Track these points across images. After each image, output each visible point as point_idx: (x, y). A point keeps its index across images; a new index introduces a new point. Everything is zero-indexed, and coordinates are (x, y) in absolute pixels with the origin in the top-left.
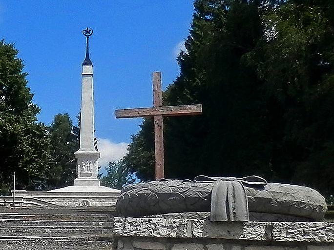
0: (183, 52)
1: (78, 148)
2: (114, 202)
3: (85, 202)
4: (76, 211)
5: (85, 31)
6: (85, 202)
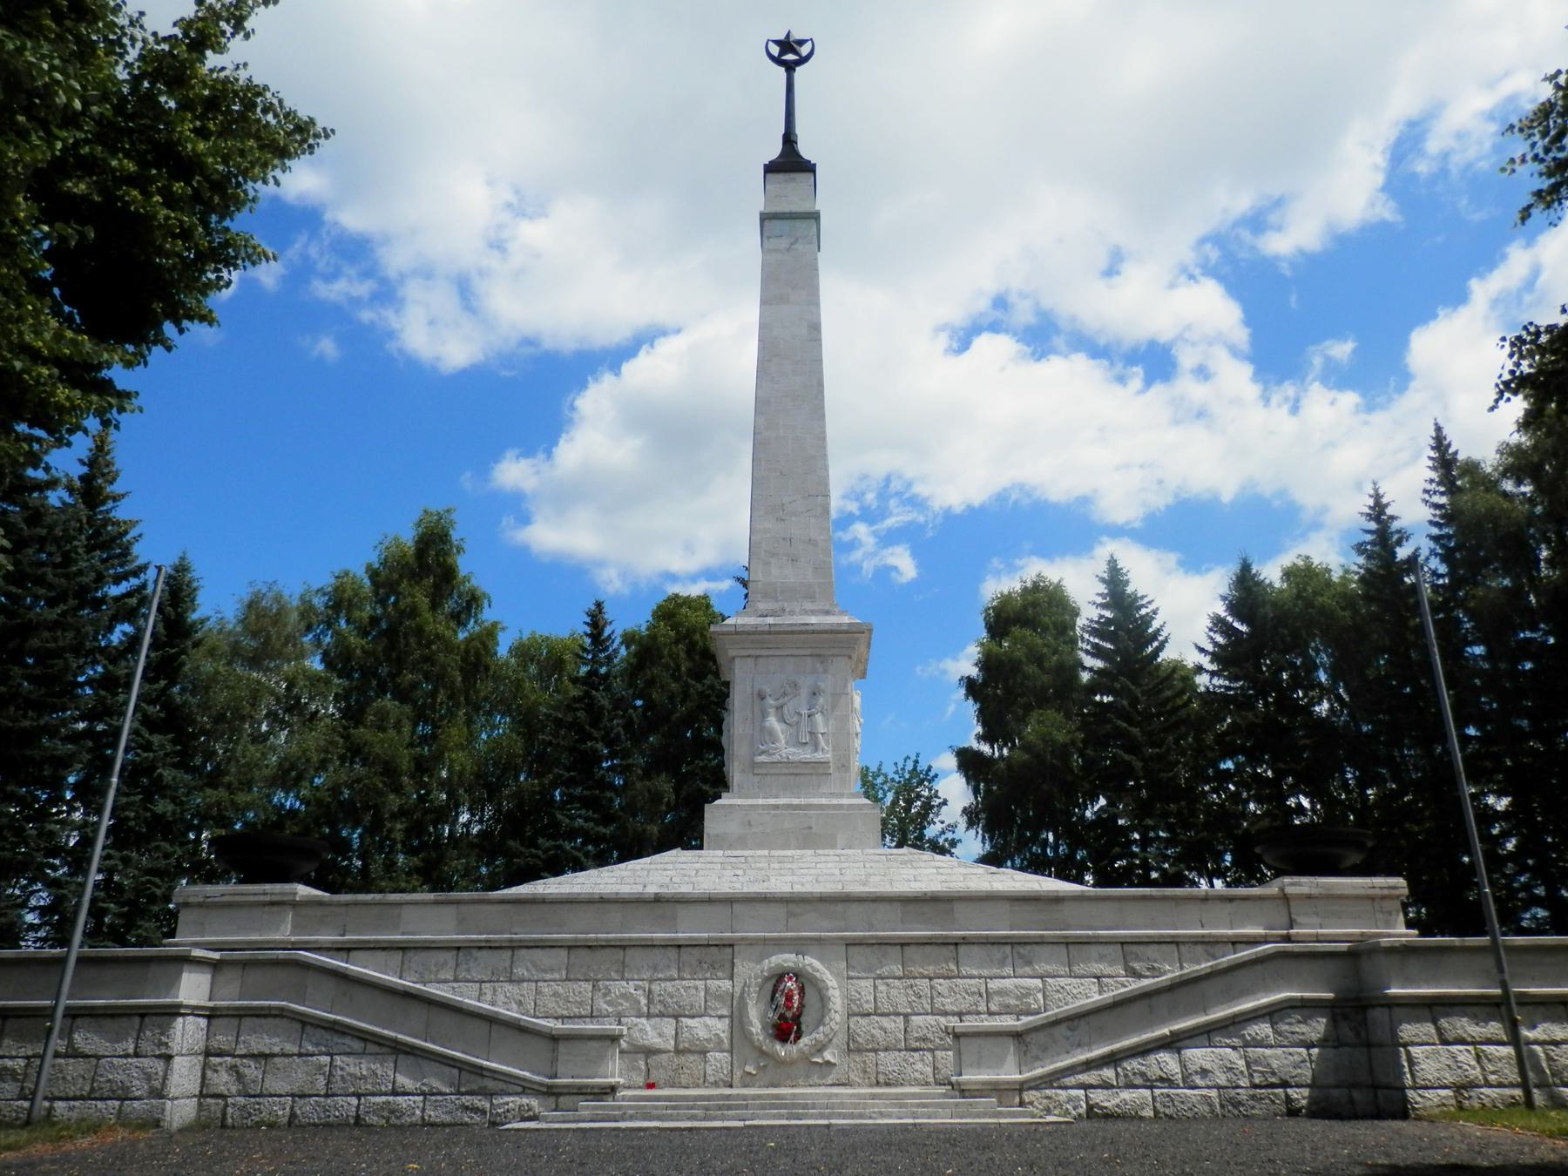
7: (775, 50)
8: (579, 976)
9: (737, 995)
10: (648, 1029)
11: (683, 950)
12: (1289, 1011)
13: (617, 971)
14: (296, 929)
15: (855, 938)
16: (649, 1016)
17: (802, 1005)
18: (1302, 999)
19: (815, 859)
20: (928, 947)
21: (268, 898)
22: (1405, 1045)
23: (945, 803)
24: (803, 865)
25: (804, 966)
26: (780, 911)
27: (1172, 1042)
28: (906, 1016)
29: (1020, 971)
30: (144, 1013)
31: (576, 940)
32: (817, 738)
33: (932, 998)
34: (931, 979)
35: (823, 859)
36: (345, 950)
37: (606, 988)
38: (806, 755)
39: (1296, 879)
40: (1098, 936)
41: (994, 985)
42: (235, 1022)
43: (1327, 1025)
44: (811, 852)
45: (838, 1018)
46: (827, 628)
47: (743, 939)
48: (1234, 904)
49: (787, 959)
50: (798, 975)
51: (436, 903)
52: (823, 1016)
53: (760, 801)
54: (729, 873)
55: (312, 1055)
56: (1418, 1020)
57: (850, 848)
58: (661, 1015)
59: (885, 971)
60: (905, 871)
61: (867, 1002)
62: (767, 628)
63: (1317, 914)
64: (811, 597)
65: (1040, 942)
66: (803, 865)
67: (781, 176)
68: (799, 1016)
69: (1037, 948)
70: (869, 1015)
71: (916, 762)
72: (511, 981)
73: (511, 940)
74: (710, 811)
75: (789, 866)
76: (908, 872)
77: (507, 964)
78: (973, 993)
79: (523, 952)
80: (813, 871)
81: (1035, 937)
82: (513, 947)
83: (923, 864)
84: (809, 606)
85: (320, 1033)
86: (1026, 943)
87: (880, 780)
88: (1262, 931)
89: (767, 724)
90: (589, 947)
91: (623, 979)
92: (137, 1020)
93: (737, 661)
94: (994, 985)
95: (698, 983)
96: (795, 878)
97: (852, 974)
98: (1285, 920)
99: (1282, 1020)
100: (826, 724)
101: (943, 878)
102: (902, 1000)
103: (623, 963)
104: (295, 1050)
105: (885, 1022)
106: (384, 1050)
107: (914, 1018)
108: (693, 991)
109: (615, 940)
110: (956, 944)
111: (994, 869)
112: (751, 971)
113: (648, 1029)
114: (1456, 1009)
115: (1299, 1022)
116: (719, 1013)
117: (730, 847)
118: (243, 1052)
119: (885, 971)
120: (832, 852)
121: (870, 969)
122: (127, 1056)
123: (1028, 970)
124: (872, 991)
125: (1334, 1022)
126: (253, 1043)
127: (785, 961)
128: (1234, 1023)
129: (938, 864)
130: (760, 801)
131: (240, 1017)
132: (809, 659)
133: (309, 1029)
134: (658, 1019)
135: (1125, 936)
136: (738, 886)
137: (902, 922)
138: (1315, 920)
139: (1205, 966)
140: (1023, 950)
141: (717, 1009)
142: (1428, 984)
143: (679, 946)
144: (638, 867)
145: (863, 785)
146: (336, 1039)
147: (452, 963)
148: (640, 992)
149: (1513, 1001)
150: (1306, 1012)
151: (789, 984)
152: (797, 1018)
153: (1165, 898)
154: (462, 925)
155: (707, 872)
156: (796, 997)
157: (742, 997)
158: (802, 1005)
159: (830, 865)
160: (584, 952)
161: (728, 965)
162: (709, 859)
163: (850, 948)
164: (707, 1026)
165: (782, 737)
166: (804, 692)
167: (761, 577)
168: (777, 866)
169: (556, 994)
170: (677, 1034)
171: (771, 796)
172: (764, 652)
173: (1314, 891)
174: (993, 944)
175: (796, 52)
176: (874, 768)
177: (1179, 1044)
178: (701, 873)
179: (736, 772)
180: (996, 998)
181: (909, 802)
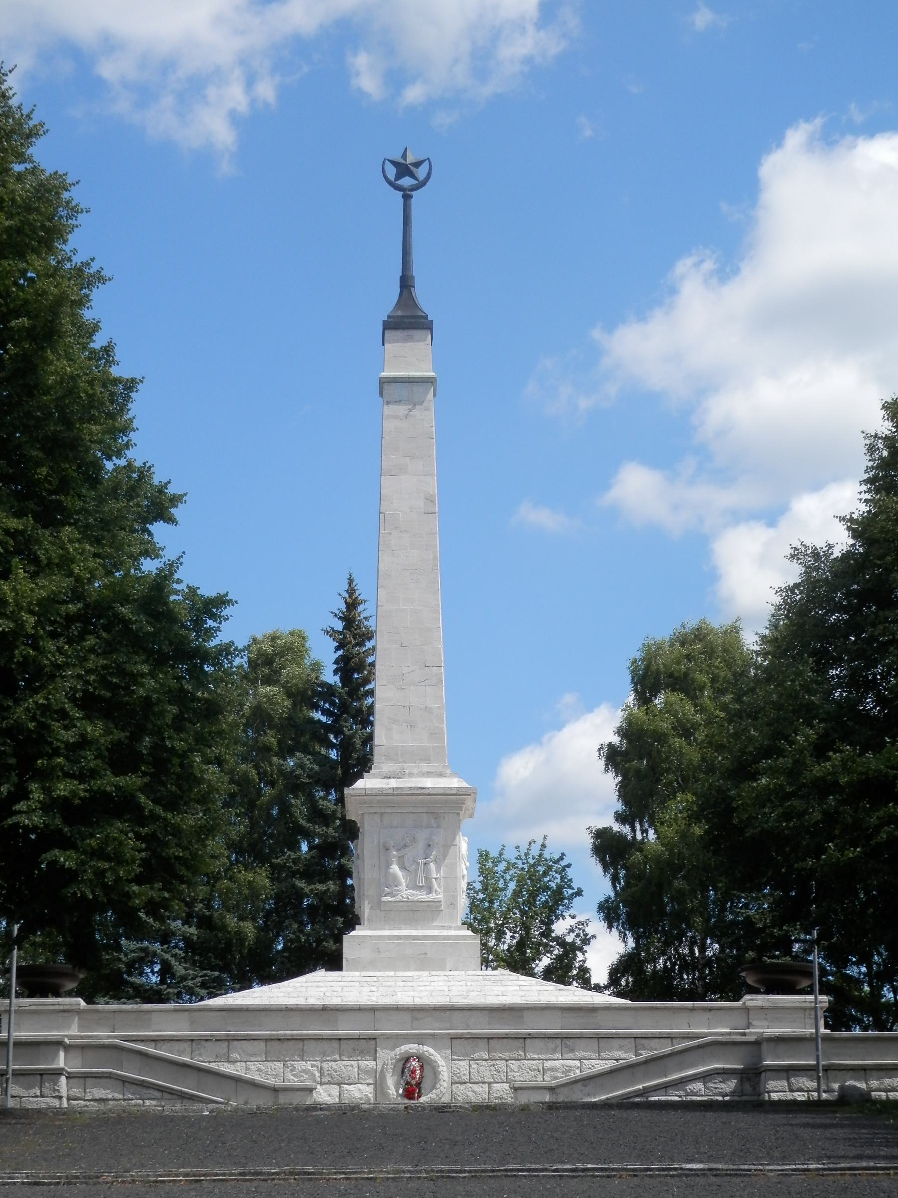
0: (11, 89)
1: (364, 764)
2: (731, 1085)
3: (414, 1063)
4: (790, 1172)
5: (394, 163)
6: (414, 1063)
7: (391, 172)
8: (273, 1059)
9: (379, 1070)
10: (322, 1091)
11: (342, 1042)
12: (716, 1075)
13: (299, 1056)
14: (81, 1027)
15: (457, 1034)
16: (321, 1084)
17: (421, 1077)
18: (724, 1069)
19: (429, 979)
20: (505, 1040)
21: (61, 1008)
22: (769, 1092)
23: (579, 892)
24: (421, 984)
25: (423, 1052)
26: (407, 1017)
27: (644, 1093)
28: (490, 1083)
29: (566, 1056)
30: (42, 1074)
31: (271, 1035)
32: (431, 882)
33: (507, 1073)
34: (507, 1061)
35: (435, 978)
36: (142, 1040)
37: (293, 1066)
38: (422, 896)
39: (754, 996)
40: (619, 1034)
41: (548, 1064)
42: (82, 1081)
43: (737, 1084)
44: (426, 973)
45: (445, 1084)
46: (440, 791)
47: (382, 1035)
48: (713, 1012)
49: (412, 1048)
50: (419, 1058)
51: (176, 1011)
52: (436, 1083)
53: (387, 933)
54: (366, 990)
55: (132, 1100)
56: (780, 1079)
57: (456, 970)
58: (329, 1083)
59: (476, 1056)
60: (496, 989)
61: (464, 1075)
62: (390, 792)
63: (766, 1019)
64: (427, 760)
65: (580, 1037)
66: (421, 984)
67: (399, 334)
68: (420, 1084)
69: (578, 1041)
70: (465, 1083)
71: (544, 846)
72: (229, 1062)
73: (228, 1035)
74: (345, 938)
75: (410, 984)
76: (498, 989)
77: (226, 1050)
78: (534, 1070)
79: (236, 1043)
80: (428, 988)
81: (576, 1033)
82: (229, 1040)
83: (510, 983)
84: (425, 767)
85: (134, 1088)
86: (571, 1038)
87: (502, 866)
88: (728, 1030)
89: (391, 870)
90: (280, 1040)
91: (303, 1060)
92: (39, 1077)
93: (366, 816)
94: (548, 1064)
95: (353, 1063)
96: (415, 994)
97: (455, 1057)
98: (744, 1023)
99: (710, 1081)
100: (438, 870)
101: (523, 993)
102: (487, 1074)
103: (303, 1050)
104: (121, 1097)
105: (475, 1087)
106: (174, 1097)
107: (495, 1085)
108: (351, 1068)
109: (297, 1035)
110: (525, 1038)
111: (562, 987)
112: (387, 1056)
113: (322, 1091)
114: (801, 1072)
115: (721, 1082)
116: (367, 1081)
117: (364, 969)
118: (90, 1097)
119: (476, 1056)
120: (442, 973)
121: (466, 1055)
122: (37, 1096)
123: (571, 1055)
124: (468, 1068)
125: (741, 1082)
126: (95, 1093)
127: (410, 1049)
128: (681, 1082)
129: (521, 983)
130: (387, 933)
131: (85, 1078)
132: (425, 815)
133: (126, 1084)
134: (327, 1085)
135: (637, 1033)
136: (374, 999)
137: (489, 1024)
138: (765, 1023)
139: (668, 1049)
140: (569, 1042)
141: (366, 1079)
142: (789, 1059)
143: (340, 1039)
144: (298, 985)
145: (482, 873)
146: (144, 1091)
147: (189, 1050)
148: (314, 1068)
149: (821, 1068)
150: (725, 1076)
151: (413, 1063)
152: (418, 1084)
153: (665, 1009)
154: (193, 1026)
155: (350, 989)
156: (418, 1072)
157: (382, 1072)
158: (421, 1077)
159: (440, 984)
160: (276, 1043)
161: (373, 1052)
162: (350, 979)
163: (454, 1040)
164: (359, 1090)
165: (403, 881)
166: (421, 845)
167: (384, 742)
168: (401, 984)
169: (259, 1070)
170: (340, 1094)
171: (394, 929)
172: (389, 810)
173: (765, 1004)
174: (549, 1038)
175: (413, 176)
176: (494, 853)
177: (647, 1094)
178: (345, 989)
179: (365, 909)
180: (549, 1072)
181: (533, 895)
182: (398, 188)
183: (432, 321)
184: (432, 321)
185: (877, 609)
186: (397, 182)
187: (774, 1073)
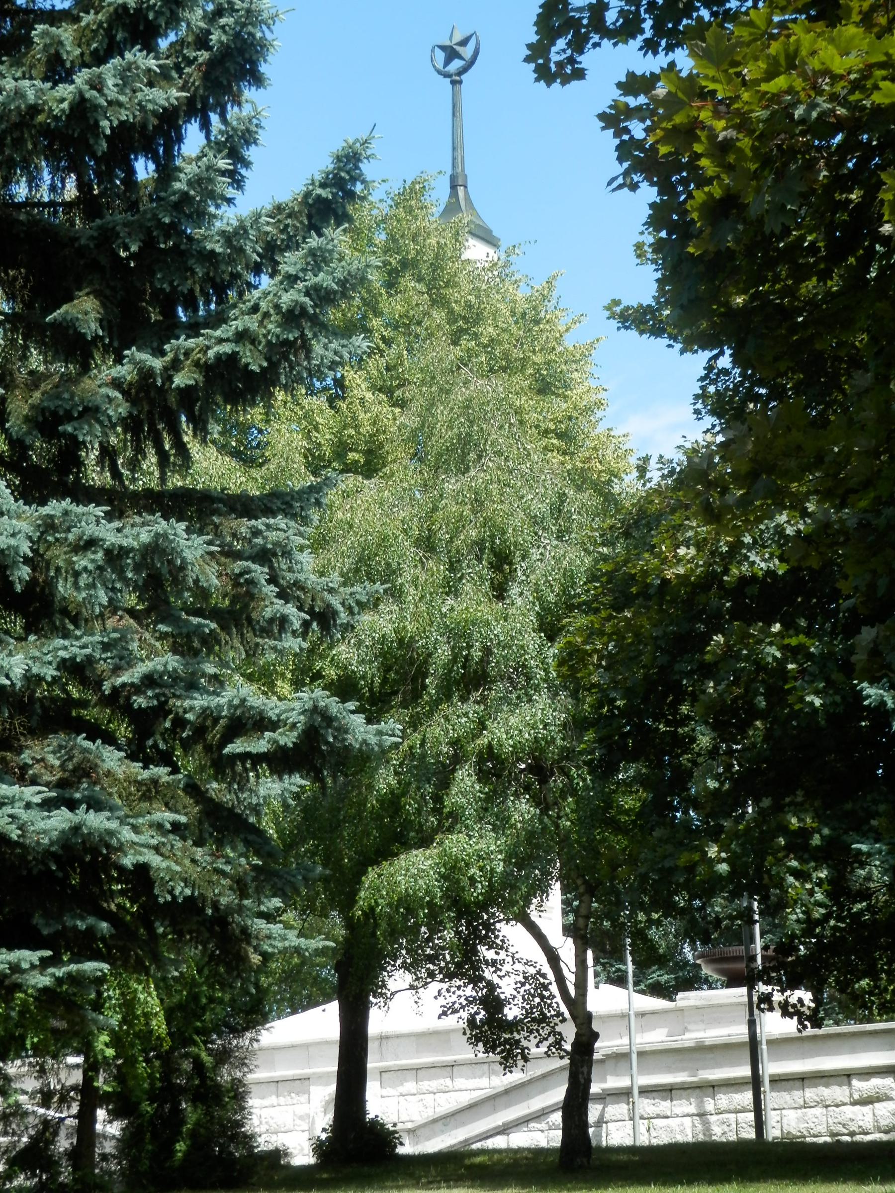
5: (443, 48)
7: (440, 56)
47: (314, 1074)
63: (702, 1021)
175: (460, 57)
182: (446, 75)
183: (540, 7)
184: (540, 7)
185: (681, 681)
186: (447, 69)
187: (613, 1098)
